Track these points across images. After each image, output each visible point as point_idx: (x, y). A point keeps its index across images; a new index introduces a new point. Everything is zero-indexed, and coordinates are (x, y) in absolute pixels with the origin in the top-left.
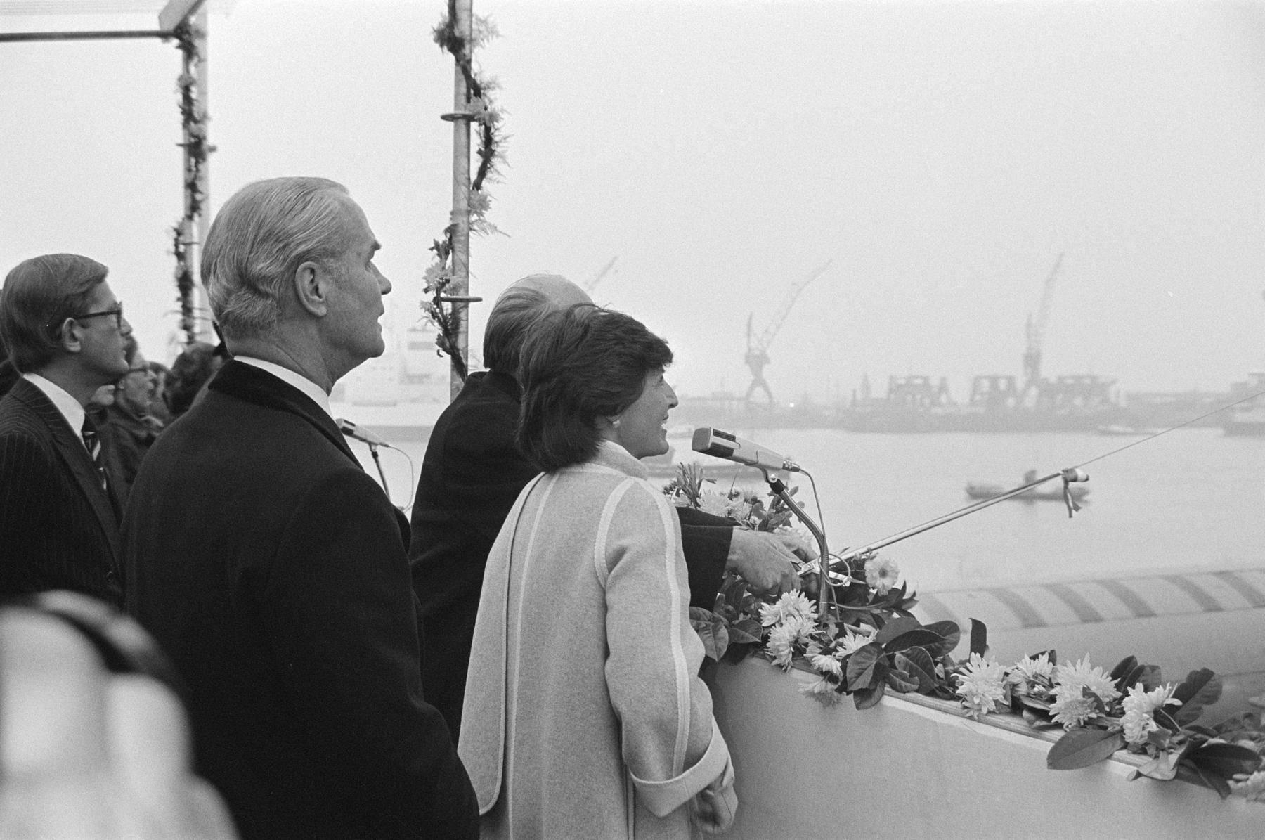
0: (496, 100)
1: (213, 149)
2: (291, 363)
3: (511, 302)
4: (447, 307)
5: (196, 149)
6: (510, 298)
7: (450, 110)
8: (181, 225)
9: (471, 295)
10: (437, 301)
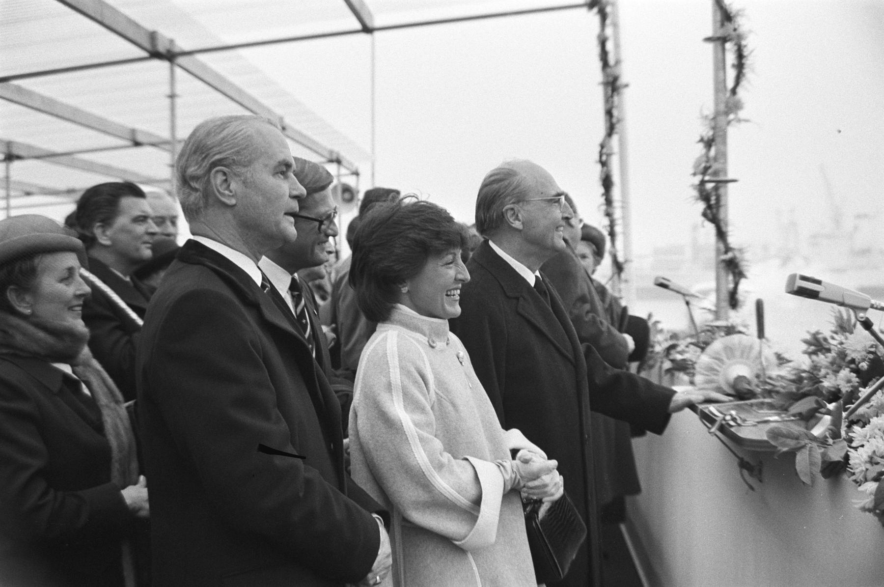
0: (743, 24)
1: (626, 86)
2: (214, 236)
3: (492, 178)
4: (709, 186)
5: (612, 85)
6: (491, 176)
7: (710, 34)
8: (604, 141)
9: (730, 176)
10: (703, 183)
